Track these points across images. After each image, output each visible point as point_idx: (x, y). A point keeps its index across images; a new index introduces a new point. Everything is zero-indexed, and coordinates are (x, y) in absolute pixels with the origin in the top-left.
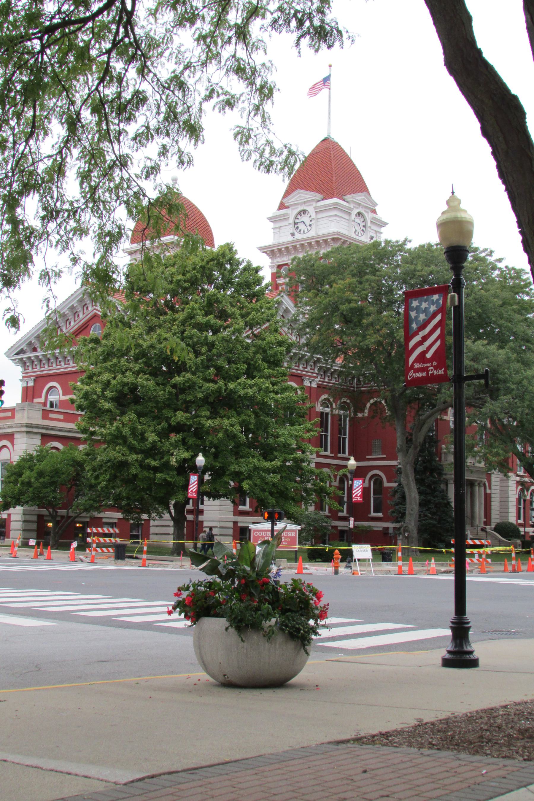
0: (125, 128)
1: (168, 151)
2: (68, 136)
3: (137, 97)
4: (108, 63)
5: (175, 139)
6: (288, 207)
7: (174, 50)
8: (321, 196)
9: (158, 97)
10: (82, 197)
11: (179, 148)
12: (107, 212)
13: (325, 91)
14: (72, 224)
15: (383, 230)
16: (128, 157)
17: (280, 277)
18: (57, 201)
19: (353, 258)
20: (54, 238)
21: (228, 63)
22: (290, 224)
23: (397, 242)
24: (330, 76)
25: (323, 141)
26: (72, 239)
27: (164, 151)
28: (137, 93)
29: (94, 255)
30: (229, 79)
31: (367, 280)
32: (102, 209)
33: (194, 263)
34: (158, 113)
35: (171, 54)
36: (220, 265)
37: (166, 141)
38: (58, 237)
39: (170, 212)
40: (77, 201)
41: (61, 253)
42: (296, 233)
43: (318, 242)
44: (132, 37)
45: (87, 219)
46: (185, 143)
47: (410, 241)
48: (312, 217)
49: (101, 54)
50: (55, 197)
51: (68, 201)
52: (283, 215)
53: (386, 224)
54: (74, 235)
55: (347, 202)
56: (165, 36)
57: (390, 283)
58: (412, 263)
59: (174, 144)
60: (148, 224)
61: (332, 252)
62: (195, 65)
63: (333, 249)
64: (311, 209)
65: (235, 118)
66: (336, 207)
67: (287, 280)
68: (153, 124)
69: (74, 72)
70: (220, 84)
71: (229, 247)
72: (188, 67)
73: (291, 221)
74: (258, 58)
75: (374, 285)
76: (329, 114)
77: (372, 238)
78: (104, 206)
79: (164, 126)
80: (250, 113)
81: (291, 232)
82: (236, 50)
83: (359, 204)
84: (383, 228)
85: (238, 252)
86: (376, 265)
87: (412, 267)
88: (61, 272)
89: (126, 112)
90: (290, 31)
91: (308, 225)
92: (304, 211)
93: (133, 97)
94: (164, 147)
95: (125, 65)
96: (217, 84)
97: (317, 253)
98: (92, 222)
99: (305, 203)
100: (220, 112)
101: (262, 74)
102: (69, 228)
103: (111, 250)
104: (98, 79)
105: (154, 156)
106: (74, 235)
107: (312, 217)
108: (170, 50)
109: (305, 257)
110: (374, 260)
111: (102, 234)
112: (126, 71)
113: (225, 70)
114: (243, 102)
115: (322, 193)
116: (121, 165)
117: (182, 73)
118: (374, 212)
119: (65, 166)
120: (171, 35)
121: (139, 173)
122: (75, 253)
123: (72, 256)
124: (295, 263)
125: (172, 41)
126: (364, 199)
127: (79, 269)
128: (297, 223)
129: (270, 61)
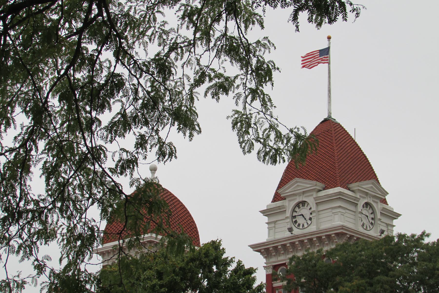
0: (97, 117)
1: (146, 142)
2: (33, 126)
3: (112, 82)
4: (79, 43)
5: (155, 128)
6: (284, 199)
7: (157, 30)
8: (323, 185)
9: (135, 81)
10: (49, 195)
11: (159, 138)
12: (77, 212)
13: (322, 68)
14: (37, 226)
15: (395, 222)
16: (101, 149)
17: (276, 280)
18: (20, 201)
19: (361, 255)
20: (15, 243)
21: (219, 43)
22: (287, 218)
23: (413, 236)
24: (328, 48)
25: (323, 122)
26: (35, 243)
27: (142, 142)
28: (112, 75)
29: (61, 260)
30: (221, 61)
31: (379, 282)
32: (72, 209)
33: (173, 265)
34: (136, 99)
35: (153, 34)
36: (207, 268)
37: (144, 130)
38: (20, 241)
39: (150, 211)
40: (43, 200)
41: (23, 259)
42: (294, 228)
43: (319, 238)
44: (105, 15)
45: (55, 219)
46: (171, 133)
47: (428, 235)
48: (312, 210)
49: (72, 34)
50: (19, 195)
51: (33, 200)
52: (279, 208)
53: (398, 215)
54: (38, 239)
55: (353, 191)
56: (146, 14)
57: (406, 284)
58: (430, 260)
59: (154, 134)
60: (125, 226)
61: (335, 250)
62: (182, 45)
63: (337, 246)
64: (311, 200)
65: (228, 103)
66: (339, 197)
67: (285, 283)
68: (130, 110)
69: (39, 56)
70: (211, 67)
71: (215, 246)
72: (174, 48)
73: (288, 214)
74: (253, 34)
75: (387, 287)
76: (329, 91)
77: (382, 232)
78: (74, 205)
79: (143, 114)
80: (246, 97)
81: (289, 226)
82: (226, 27)
83: (367, 194)
84: (394, 221)
85: (226, 251)
86: (389, 264)
87: (431, 265)
88: (24, 282)
89: (99, 98)
90: (286, 4)
91: (307, 218)
92: (303, 203)
93: (107, 81)
94: (142, 137)
95: (98, 46)
96: (208, 67)
97: (318, 251)
98: (60, 223)
99: (304, 193)
100: (213, 97)
101: (257, 53)
102: (32, 231)
103: (83, 256)
104: (67, 61)
105: (131, 148)
106: (38, 239)
107: (312, 210)
108: (153, 29)
109: (306, 256)
110: (386, 258)
111: (71, 237)
112: (100, 52)
113: (215, 51)
114: (238, 86)
115: (323, 182)
116: (94, 158)
117: (167, 55)
118: (384, 201)
119: (29, 160)
120: (153, 13)
121: (114, 167)
122: (40, 259)
123: (36, 263)
124: (293, 263)
125: (155, 20)
126: (372, 187)
127: (44, 278)
128: (295, 217)
129: (266, 38)
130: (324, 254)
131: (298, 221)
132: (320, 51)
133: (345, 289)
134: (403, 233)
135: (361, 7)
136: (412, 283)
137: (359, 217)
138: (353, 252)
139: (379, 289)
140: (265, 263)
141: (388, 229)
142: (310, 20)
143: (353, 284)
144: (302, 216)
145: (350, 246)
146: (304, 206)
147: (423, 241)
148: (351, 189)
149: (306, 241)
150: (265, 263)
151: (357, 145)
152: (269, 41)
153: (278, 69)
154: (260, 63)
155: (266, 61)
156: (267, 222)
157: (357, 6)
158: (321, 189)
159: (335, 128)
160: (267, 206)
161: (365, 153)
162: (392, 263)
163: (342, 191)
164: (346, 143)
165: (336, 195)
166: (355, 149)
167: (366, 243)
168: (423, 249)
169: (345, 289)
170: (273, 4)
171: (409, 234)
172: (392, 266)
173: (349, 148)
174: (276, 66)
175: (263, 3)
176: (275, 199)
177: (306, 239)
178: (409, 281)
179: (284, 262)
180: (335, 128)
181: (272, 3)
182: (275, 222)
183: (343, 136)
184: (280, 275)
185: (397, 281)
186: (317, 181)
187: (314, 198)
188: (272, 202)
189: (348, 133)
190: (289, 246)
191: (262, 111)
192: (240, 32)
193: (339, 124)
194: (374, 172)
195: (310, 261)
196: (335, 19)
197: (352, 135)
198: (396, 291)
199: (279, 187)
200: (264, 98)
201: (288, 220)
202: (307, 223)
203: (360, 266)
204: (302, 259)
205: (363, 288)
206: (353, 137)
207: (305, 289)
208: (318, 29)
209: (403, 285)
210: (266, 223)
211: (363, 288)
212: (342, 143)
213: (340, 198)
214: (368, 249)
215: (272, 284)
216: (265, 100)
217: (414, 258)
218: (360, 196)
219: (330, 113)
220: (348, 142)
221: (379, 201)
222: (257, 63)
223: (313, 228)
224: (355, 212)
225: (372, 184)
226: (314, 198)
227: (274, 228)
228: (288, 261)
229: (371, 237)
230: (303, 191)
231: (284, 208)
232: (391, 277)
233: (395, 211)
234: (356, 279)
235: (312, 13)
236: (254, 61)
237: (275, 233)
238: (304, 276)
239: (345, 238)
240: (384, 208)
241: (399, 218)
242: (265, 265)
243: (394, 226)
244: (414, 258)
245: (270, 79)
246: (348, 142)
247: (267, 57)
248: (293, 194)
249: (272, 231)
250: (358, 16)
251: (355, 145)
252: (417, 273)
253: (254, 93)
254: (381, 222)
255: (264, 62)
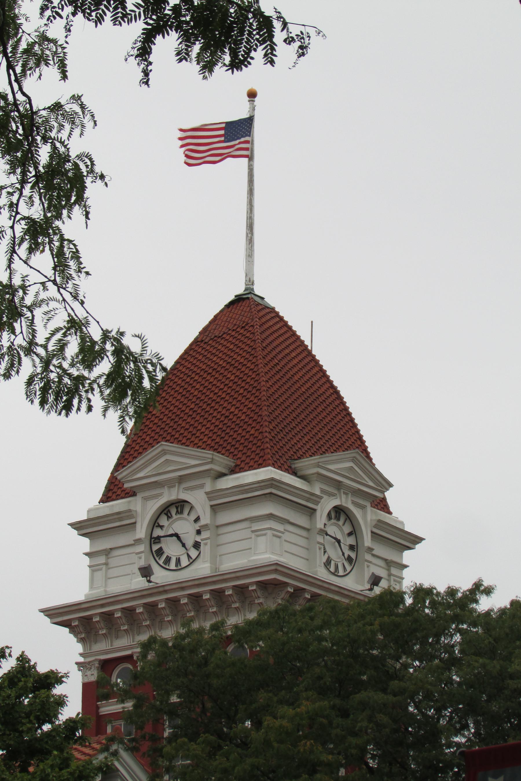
6: (132, 493)
8: (228, 461)
13: (234, 167)
15: (407, 556)
17: (106, 697)
19: (321, 639)
22: (138, 541)
23: (452, 592)
25: (232, 303)
42: (155, 568)
47: (488, 591)
48: (202, 522)
52: (118, 515)
53: (417, 540)
55: (303, 477)
58: (492, 654)
64: (198, 499)
66: (270, 492)
67: (129, 705)
73: (141, 532)
76: (250, 227)
77: (376, 581)
81: (142, 563)
83: (338, 485)
87: (495, 666)
91: (189, 543)
92: (180, 505)
97: (215, 627)
107: (202, 522)
115: (229, 453)
118: (382, 505)
128: (158, 540)
129: (76, 98)
130: (229, 633)
131: (165, 549)
132: (227, 123)
133: (278, 723)
134: (426, 585)
135: (312, 32)
136: (446, 709)
137: (319, 543)
138: (300, 631)
139: (365, 724)
140: (81, 655)
141: (390, 575)
142: (182, 56)
143: (298, 710)
144: (175, 538)
145: (294, 614)
146: (182, 512)
147: (474, 605)
148: (299, 474)
149: (184, 601)
150: (81, 655)
151: (317, 362)
152: (83, 107)
153: (102, 177)
154: (59, 159)
155: (73, 154)
156: (88, 550)
157: (302, 29)
158: (224, 471)
159: (264, 320)
160: (89, 511)
161: (335, 384)
162: (397, 659)
163: (277, 477)
164: (289, 358)
165: (261, 488)
166: (311, 374)
167: (333, 608)
168: (475, 626)
169: (278, 723)
170: (94, 14)
171: (442, 589)
172: (398, 666)
173: (295, 370)
174: (98, 169)
175: (69, 9)
176: (110, 494)
177: (184, 596)
178: (439, 704)
179: (129, 652)
180: (264, 320)
181: (92, 11)
182: (107, 552)
183: (281, 339)
184: (117, 684)
185: (409, 704)
186: (215, 450)
187: (207, 493)
188: (102, 501)
189: (294, 333)
190: (162, 608)
191: (54, 282)
192: (13, 78)
193: (273, 309)
194: (358, 431)
195: (193, 651)
196: (245, 59)
197: (304, 336)
198: (407, 729)
199: (120, 465)
200: (62, 247)
201: (141, 548)
202: (189, 556)
203: (318, 664)
204: (174, 646)
205: (325, 721)
206: (307, 342)
207: (179, 722)
208: (205, 78)
209: (424, 715)
210: (86, 554)
211: (325, 721)
212: (280, 357)
213: (271, 493)
214: (339, 623)
215: (98, 708)
216: (64, 254)
217: (453, 646)
218: (322, 491)
219: (250, 283)
220: (294, 354)
221: (368, 505)
222: (51, 157)
223: (202, 569)
224: (308, 530)
225: (353, 461)
226: (207, 493)
227: (104, 567)
228: (139, 650)
229: (346, 592)
230: (180, 476)
231: (132, 517)
232: (395, 695)
233: (407, 529)
234: (307, 699)
235: (188, 38)
236: (44, 154)
237: (107, 578)
238: (177, 688)
239: (283, 595)
240: (379, 521)
241: (417, 546)
242: (81, 660)
243: (406, 566)
244: (453, 646)
245: (80, 199)
246: (294, 354)
247: (76, 146)
248: (156, 482)
249: (99, 575)
250: (303, 54)
251: (312, 364)
252: (459, 683)
253: (38, 232)
254: (374, 555)
255: (66, 158)
